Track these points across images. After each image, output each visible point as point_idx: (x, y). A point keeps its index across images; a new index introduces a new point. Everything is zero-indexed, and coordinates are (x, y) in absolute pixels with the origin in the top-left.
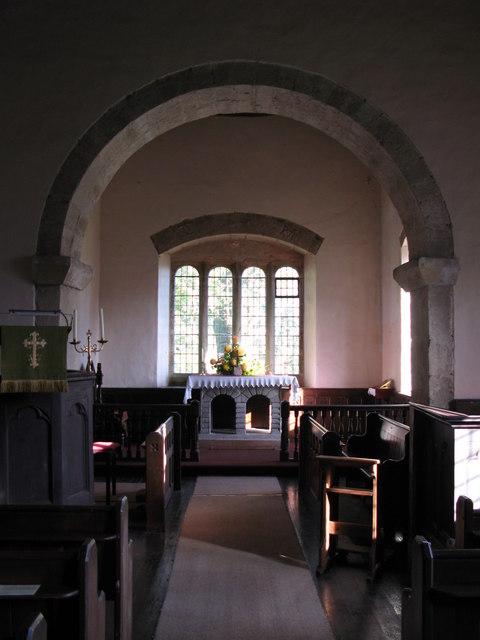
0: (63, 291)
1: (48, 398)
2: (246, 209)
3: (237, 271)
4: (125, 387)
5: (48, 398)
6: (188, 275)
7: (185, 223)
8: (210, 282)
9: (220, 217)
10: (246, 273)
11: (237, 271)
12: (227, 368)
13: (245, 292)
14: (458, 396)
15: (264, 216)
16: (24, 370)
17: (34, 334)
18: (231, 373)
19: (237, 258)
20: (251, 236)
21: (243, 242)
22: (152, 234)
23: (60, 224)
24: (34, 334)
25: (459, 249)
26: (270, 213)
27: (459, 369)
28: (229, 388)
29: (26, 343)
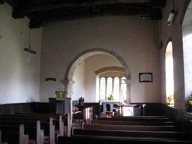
0: (68, 85)
1: (63, 101)
2: (114, 66)
3: (113, 78)
4: (90, 102)
5: (63, 101)
6: (103, 79)
7: (101, 69)
8: (108, 80)
9: (109, 67)
10: (108, 79)
11: (113, 78)
12: (110, 99)
13: (115, 83)
14: (131, 102)
15: (118, 67)
16: (59, 97)
17: (61, 92)
18: (110, 100)
19: (113, 76)
20: (115, 71)
21: (114, 72)
22: (95, 71)
23: (68, 75)
24: (61, 92)
25: (132, 77)
26: (119, 66)
27: (132, 98)
28: (109, 103)
29: (60, 93)
